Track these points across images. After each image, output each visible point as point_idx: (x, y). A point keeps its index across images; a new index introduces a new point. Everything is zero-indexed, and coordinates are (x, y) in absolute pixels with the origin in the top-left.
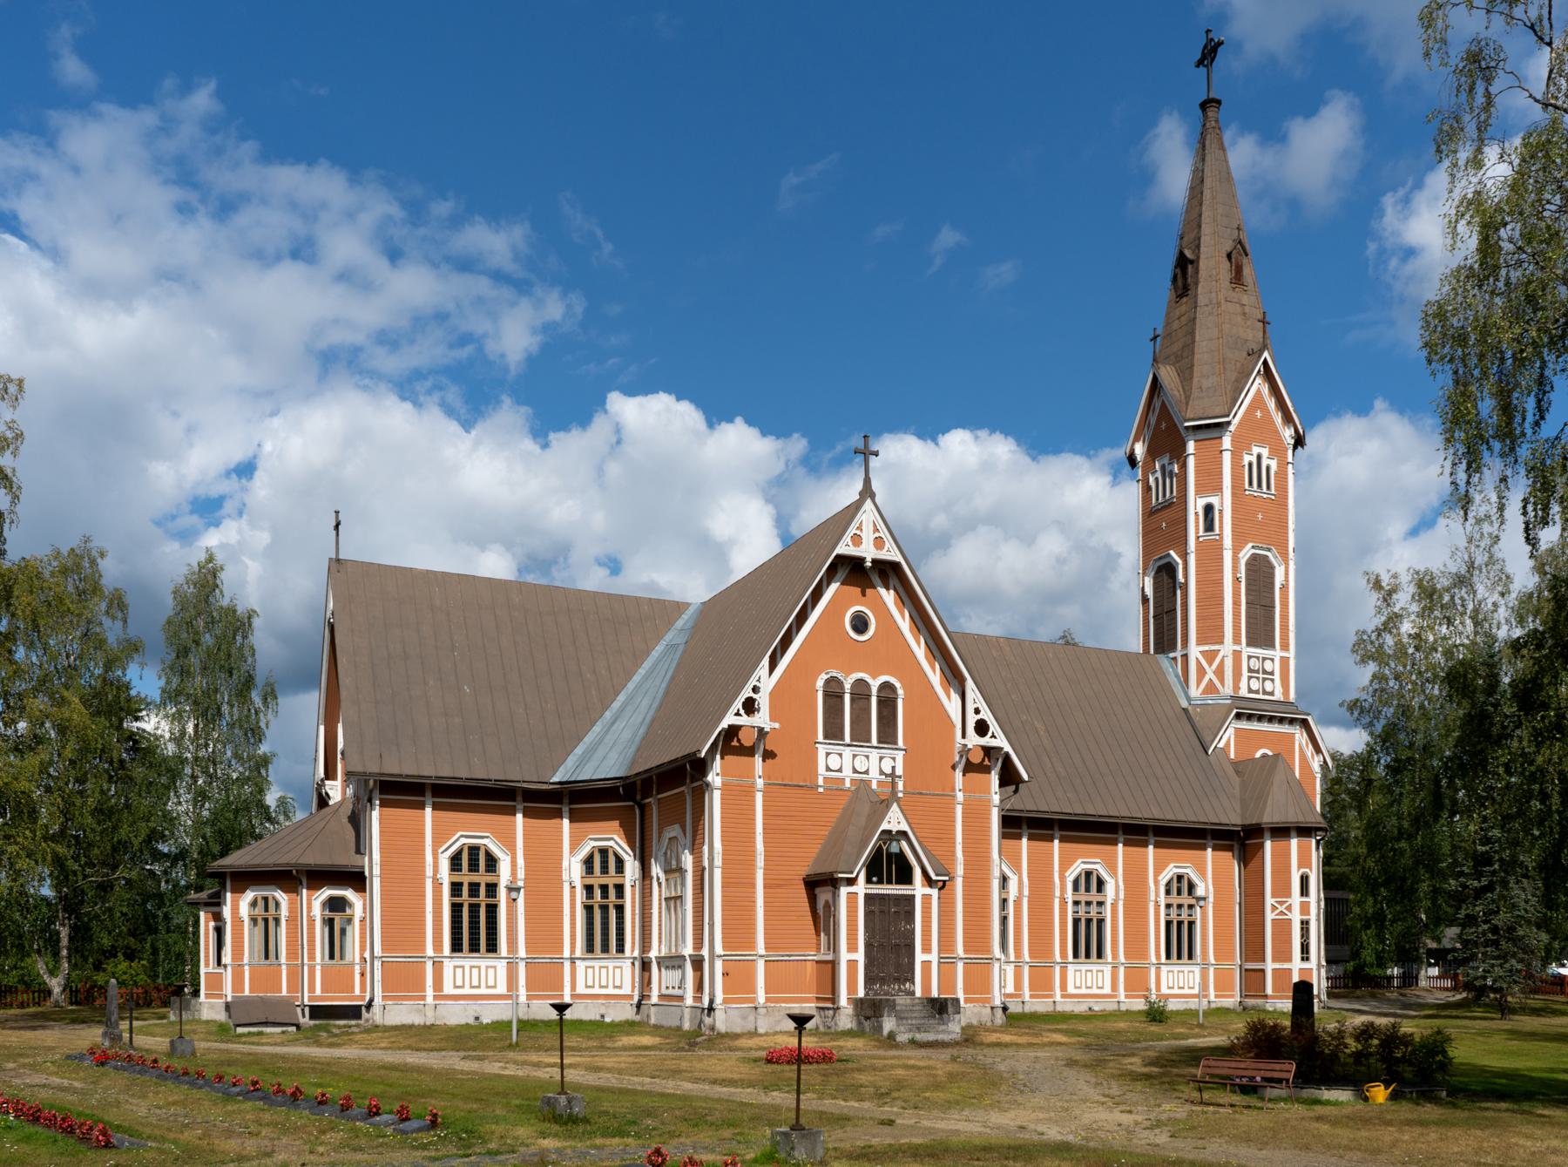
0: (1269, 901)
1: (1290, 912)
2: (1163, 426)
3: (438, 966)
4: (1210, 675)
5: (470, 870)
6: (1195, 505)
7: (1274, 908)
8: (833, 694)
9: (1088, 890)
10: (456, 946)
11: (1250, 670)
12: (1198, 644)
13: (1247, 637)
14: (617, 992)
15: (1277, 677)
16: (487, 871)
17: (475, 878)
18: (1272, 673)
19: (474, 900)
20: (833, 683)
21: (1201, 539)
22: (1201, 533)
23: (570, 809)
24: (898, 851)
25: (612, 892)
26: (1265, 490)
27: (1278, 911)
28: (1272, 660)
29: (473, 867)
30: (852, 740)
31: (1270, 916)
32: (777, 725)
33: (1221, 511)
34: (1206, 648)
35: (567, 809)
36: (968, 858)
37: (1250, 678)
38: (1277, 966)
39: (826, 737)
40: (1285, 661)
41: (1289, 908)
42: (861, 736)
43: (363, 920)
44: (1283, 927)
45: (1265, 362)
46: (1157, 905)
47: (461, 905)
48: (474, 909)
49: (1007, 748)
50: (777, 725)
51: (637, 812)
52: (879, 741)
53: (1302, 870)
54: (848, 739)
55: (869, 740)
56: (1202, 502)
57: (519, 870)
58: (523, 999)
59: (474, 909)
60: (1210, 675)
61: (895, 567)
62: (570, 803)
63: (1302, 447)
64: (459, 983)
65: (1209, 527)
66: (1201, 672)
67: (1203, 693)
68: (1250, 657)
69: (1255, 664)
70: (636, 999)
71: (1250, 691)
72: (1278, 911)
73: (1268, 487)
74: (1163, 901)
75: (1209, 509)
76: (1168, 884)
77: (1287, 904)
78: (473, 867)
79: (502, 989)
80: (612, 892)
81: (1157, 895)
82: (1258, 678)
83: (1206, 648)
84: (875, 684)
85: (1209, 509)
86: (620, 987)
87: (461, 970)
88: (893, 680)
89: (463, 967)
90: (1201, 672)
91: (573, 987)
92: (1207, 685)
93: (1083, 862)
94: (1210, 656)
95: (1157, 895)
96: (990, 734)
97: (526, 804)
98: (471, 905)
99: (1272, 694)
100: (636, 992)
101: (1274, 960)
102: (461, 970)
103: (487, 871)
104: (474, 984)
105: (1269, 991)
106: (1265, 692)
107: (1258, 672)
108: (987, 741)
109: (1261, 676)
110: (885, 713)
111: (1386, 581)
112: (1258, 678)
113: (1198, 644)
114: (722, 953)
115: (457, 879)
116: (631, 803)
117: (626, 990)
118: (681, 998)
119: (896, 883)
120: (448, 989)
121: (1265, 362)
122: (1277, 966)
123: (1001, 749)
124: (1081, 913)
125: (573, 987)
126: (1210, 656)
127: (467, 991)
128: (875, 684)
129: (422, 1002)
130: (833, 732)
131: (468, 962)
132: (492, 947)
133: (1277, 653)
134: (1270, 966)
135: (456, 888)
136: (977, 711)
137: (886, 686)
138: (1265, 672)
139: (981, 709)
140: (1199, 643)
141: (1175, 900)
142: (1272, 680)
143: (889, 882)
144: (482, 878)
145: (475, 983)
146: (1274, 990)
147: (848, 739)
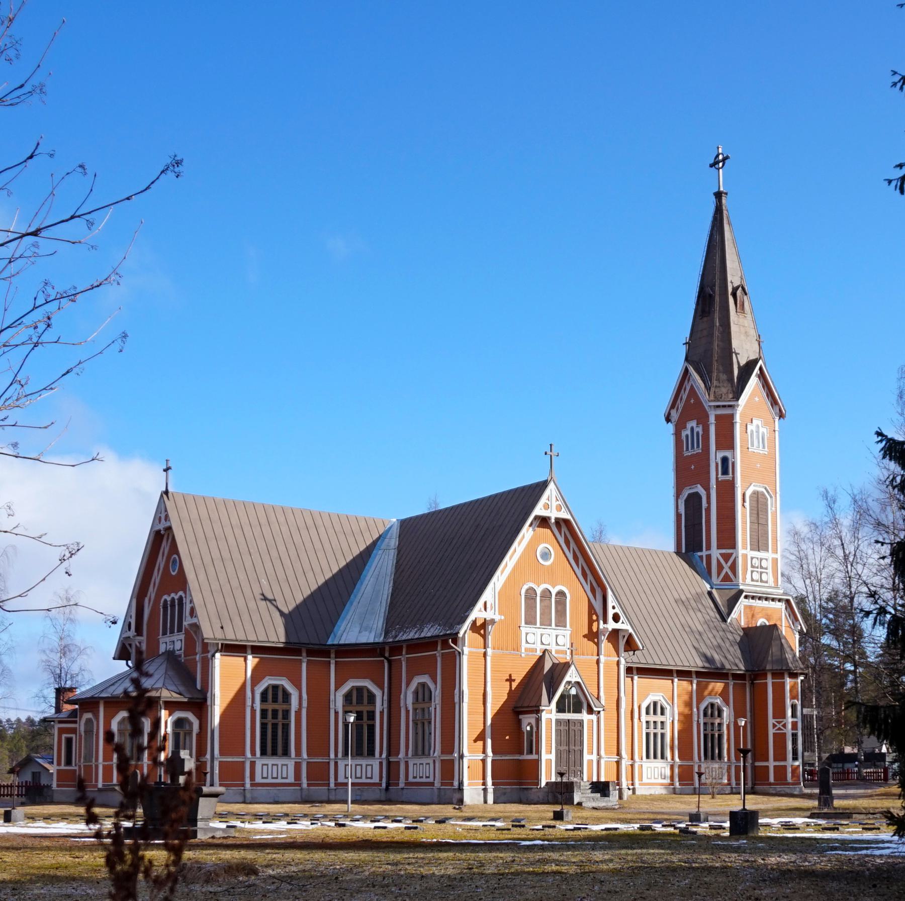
0: (771, 721)
1: (785, 728)
2: (692, 401)
3: (253, 764)
4: (726, 569)
5: (273, 702)
6: (715, 457)
7: (774, 726)
8: (531, 595)
9: (655, 713)
10: (264, 753)
11: (752, 566)
12: (718, 548)
13: (751, 545)
14: (369, 781)
15: (770, 571)
16: (283, 702)
17: (276, 706)
18: (766, 569)
19: (275, 721)
20: (530, 591)
21: (720, 480)
22: (720, 476)
23: (336, 661)
24: (575, 693)
25: (659, 725)
26: (761, 448)
27: (776, 728)
28: (767, 560)
29: (275, 700)
30: (541, 625)
31: (771, 731)
32: (503, 617)
33: (733, 464)
34: (724, 551)
35: (305, 660)
36: (470, 680)
37: (752, 572)
38: (777, 763)
39: (526, 623)
40: (775, 561)
41: (784, 726)
42: (546, 623)
43: (199, 735)
44: (780, 739)
45: (761, 369)
46: (698, 724)
47: (266, 724)
48: (275, 726)
49: (631, 631)
50: (503, 617)
51: (386, 665)
52: (556, 626)
53: (792, 701)
54: (538, 625)
55: (550, 625)
56: (721, 454)
57: (304, 702)
58: (305, 785)
59: (275, 726)
60: (726, 569)
61: (567, 522)
62: (336, 658)
63: (784, 419)
64: (265, 775)
65: (725, 472)
66: (720, 568)
67: (721, 581)
68: (752, 558)
69: (756, 562)
70: (384, 785)
71: (752, 580)
72: (776, 728)
73: (764, 447)
74: (702, 721)
75: (725, 460)
76: (706, 708)
77: (783, 723)
78: (275, 700)
79: (291, 779)
80: (659, 725)
81: (698, 717)
82: (757, 572)
83: (724, 551)
84: (554, 592)
85: (725, 460)
86: (371, 778)
87: (266, 766)
88: (566, 591)
89: (267, 765)
90: (720, 568)
91: (336, 778)
92: (724, 576)
93: (663, 696)
94: (726, 557)
95: (698, 717)
96: (621, 621)
97: (309, 658)
98: (273, 724)
99: (766, 582)
100: (384, 780)
101: (775, 760)
102: (276, 766)
103: (283, 702)
104: (274, 776)
105: (772, 779)
106: (762, 581)
107: (757, 568)
108: (618, 626)
109: (759, 570)
110: (559, 608)
111: (831, 493)
112: (757, 572)
113: (718, 548)
114: (468, 755)
115: (265, 707)
116: (382, 659)
117: (376, 779)
118: (432, 784)
119: (573, 712)
120: (258, 779)
121: (761, 369)
122: (777, 763)
123: (627, 630)
124: (652, 731)
125: (336, 778)
126: (726, 557)
127: (270, 781)
128: (554, 592)
129: (243, 788)
130: (530, 621)
131: (270, 761)
132: (286, 753)
133: (769, 555)
134: (772, 764)
135: (264, 713)
136: (614, 608)
137: (561, 594)
138: (762, 567)
139: (616, 606)
140: (719, 547)
141: (652, 718)
142: (767, 573)
143: (569, 712)
144: (279, 707)
145: (275, 775)
146: (775, 779)
147: (538, 625)
